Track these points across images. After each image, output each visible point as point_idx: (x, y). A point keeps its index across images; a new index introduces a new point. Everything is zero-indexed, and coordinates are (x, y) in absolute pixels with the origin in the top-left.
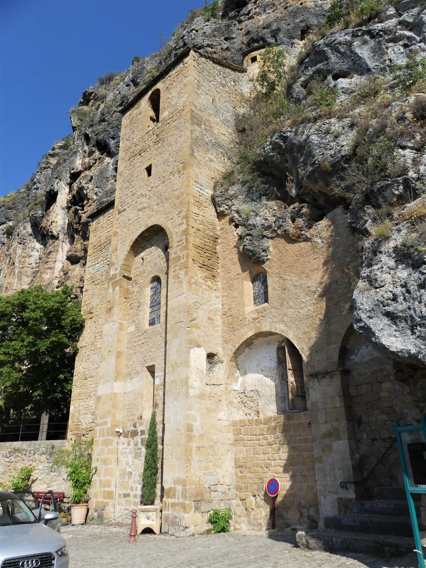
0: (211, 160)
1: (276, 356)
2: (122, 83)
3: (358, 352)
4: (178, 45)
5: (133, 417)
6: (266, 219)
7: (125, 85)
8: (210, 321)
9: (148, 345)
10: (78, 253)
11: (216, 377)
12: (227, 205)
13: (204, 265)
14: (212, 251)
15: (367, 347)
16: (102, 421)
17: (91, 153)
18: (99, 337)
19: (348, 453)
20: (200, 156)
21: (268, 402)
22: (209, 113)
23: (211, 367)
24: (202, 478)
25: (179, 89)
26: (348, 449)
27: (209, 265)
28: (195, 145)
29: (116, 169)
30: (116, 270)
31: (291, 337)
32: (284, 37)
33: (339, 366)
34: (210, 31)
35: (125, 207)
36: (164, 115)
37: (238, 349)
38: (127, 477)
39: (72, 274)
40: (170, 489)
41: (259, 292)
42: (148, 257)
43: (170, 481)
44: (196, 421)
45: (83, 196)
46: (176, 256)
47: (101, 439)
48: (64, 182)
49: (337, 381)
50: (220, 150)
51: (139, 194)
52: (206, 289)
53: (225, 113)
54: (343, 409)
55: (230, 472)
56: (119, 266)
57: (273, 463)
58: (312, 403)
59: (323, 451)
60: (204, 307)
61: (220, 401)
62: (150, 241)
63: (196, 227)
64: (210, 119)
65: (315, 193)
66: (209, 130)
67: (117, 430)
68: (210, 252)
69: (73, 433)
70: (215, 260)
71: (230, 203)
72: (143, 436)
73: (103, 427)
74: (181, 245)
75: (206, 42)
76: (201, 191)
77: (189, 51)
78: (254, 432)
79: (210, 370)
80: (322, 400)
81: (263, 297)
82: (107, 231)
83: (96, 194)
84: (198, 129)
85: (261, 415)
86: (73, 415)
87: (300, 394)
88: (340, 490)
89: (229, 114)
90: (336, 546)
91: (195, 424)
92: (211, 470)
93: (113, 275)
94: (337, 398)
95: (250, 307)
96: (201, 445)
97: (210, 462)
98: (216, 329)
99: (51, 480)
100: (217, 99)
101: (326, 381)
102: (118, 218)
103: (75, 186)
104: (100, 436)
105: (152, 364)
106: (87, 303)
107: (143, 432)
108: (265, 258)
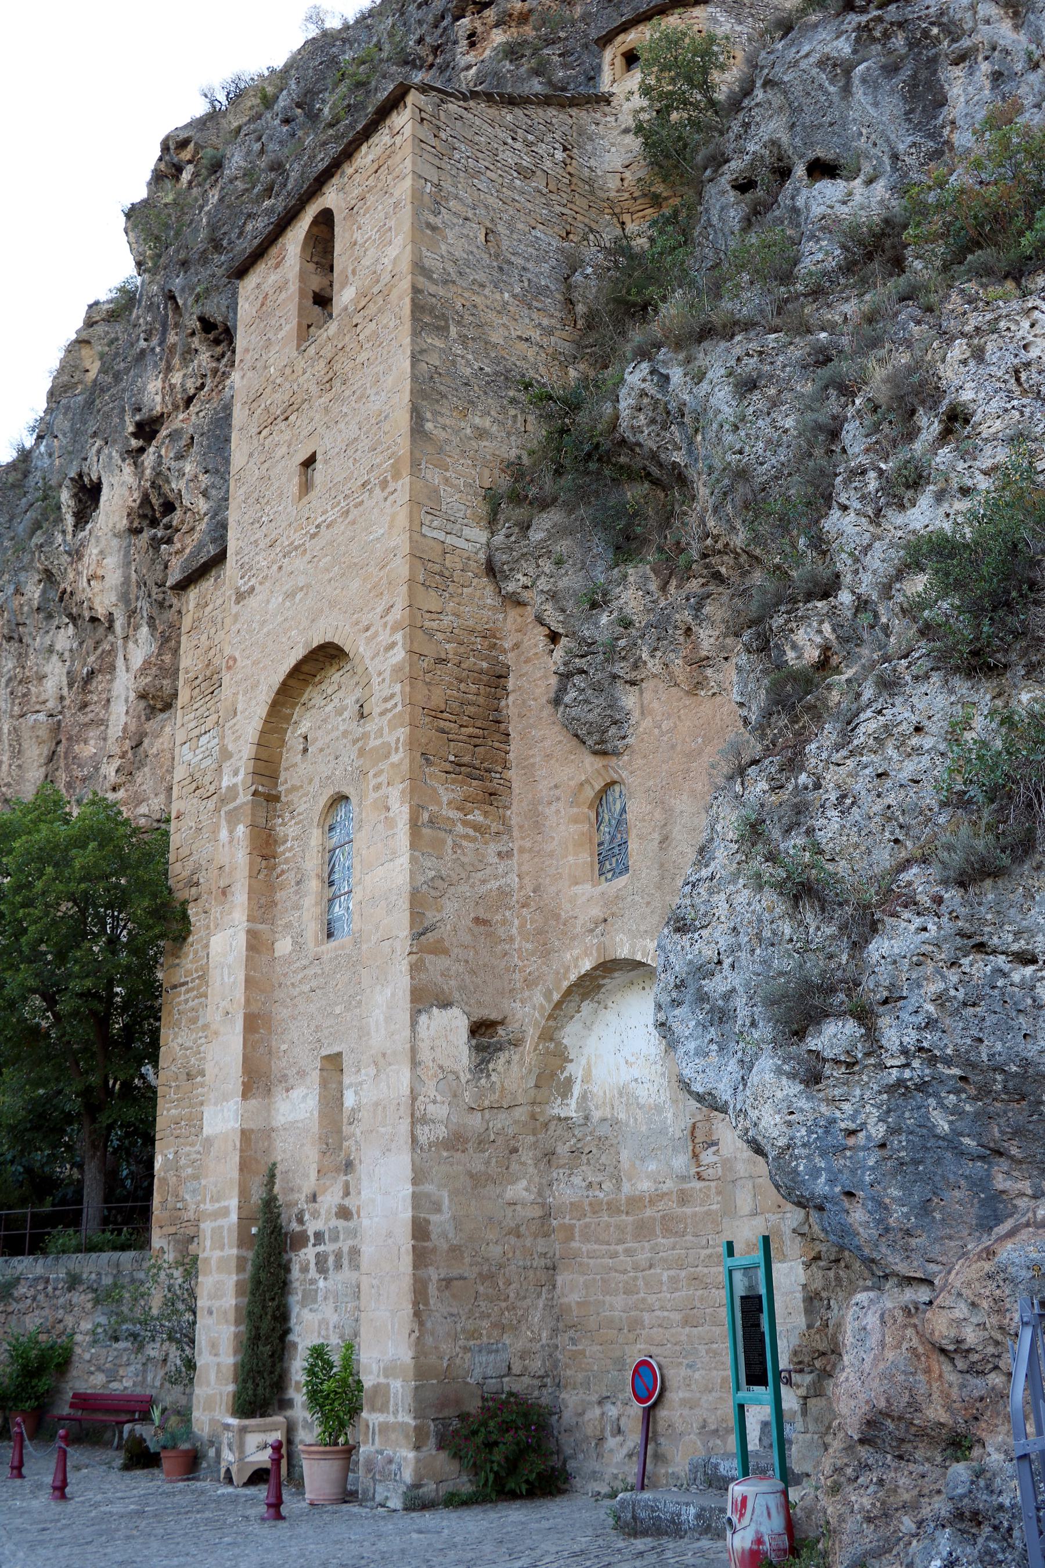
7: (277, 122)
9: (324, 994)
11: (498, 1085)
16: (217, 1205)
23: (482, 1062)
24: (458, 1361)
25: (382, 215)
27: (476, 763)
30: (236, 773)
36: (344, 297)
37: (558, 1005)
39: (152, 744)
40: (377, 1387)
43: (375, 1367)
44: (439, 1210)
45: (171, 496)
46: (378, 742)
47: (217, 1253)
52: (466, 837)
53: (530, 265)
55: (544, 1341)
56: (242, 763)
57: (646, 1316)
60: (464, 888)
61: (515, 1150)
62: (323, 686)
68: (479, 724)
70: (496, 745)
73: (220, 1222)
74: (390, 710)
83: (205, 494)
84: (439, 343)
86: (164, 1180)
91: (434, 1218)
92: (485, 1339)
93: (228, 787)
96: (455, 1273)
97: (484, 1316)
99: (117, 1362)
100: (501, 229)
103: (149, 459)
105: (336, 1049)
108: (620, 744)
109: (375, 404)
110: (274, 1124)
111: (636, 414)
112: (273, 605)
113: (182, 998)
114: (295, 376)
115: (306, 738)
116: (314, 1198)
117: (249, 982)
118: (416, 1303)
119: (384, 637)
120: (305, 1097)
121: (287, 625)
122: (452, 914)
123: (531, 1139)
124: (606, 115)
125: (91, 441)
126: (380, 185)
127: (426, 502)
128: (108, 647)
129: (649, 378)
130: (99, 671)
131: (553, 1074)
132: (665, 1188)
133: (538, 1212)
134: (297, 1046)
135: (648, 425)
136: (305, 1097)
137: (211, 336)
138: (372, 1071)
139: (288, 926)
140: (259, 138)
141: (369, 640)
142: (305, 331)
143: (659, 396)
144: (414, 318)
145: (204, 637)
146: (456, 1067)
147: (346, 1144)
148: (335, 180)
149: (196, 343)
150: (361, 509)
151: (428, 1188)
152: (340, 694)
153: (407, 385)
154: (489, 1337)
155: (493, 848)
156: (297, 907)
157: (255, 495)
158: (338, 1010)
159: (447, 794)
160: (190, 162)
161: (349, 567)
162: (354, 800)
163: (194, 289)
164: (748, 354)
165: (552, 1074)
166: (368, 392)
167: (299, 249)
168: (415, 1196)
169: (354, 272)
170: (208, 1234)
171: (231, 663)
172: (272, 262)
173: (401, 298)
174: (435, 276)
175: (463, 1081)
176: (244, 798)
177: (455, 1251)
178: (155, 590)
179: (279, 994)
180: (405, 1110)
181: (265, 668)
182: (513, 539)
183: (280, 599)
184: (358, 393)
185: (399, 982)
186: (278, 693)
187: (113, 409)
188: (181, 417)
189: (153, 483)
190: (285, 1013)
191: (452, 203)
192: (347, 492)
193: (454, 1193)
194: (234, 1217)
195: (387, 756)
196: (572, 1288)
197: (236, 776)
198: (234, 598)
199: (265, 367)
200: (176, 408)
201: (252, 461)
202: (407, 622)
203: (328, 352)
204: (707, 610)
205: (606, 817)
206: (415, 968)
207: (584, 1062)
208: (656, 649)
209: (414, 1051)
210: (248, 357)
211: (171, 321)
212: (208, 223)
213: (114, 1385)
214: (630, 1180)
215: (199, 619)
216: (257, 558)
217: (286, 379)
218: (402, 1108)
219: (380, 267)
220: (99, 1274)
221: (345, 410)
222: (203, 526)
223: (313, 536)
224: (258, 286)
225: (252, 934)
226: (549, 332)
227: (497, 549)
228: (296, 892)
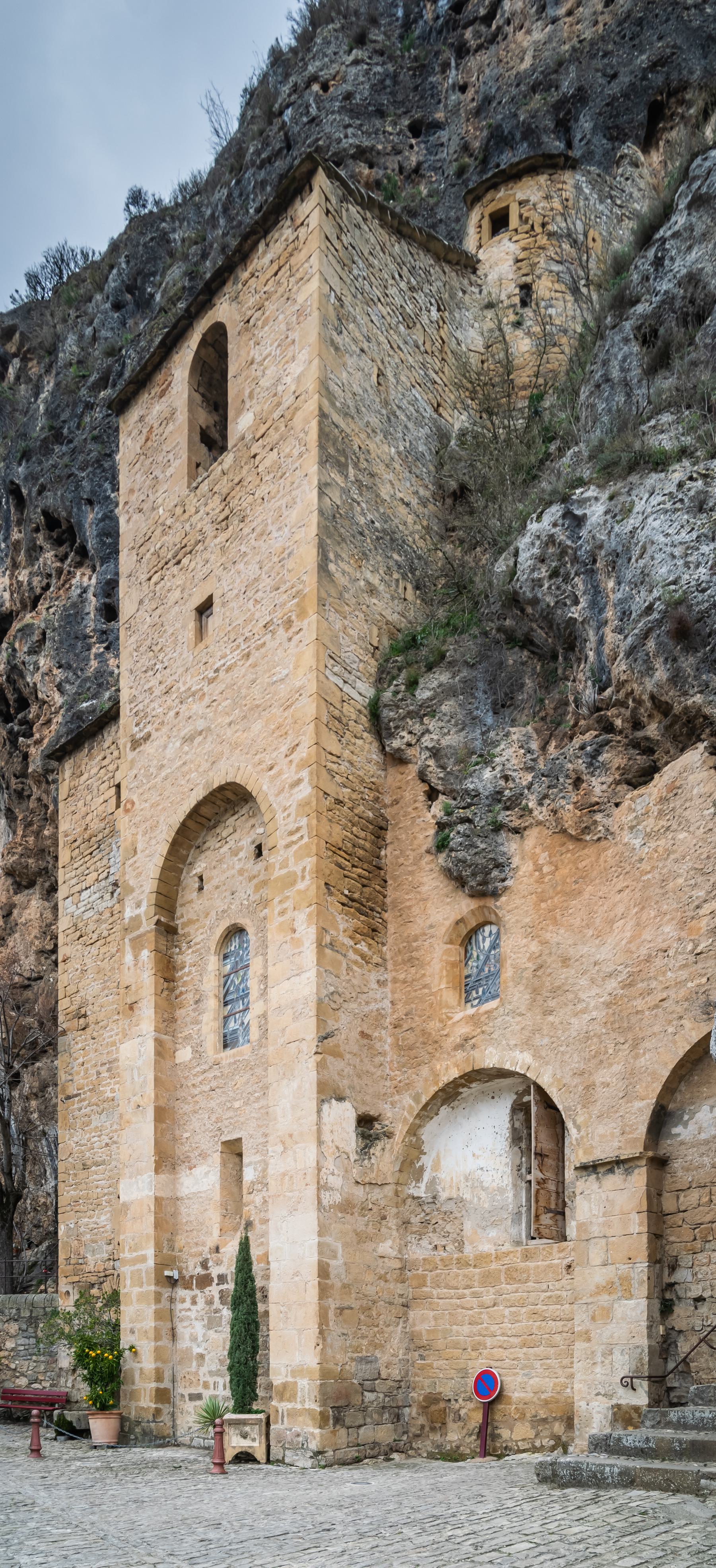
0: (372, 590)
1: (508, 1125)
2: (98, 297)
3: (691, 1118)
4: (266, 144)
5: (200, 1249)
6: (506, 778)
7: (108, 305)
8: (365, 1041)
12: (410, 733)
13: (353, 900)
14: (370, 863)
17: (34, 552)
18: (106, 1074)
19: (644, 1324)
20: (344, 572)
22: (368, 422)
25: (283, 327)
26: (645, 1316)
28: (330, 536)
29: (110, 612)
30: (138, 905)
31: (545, 1081)
32: (594, 129)
33: (646, 1148)
34: (365, 90)
35: (149, 728)
36: (241, 424)
38: (194, 1364)
40: (285, 1386)
41: (478, 974)
43: (283, 1370)
44: (335, 1257)
45: (26, 692)
46: (284, 872)
47: (136, 1290)
49: (639, 1178)
50: (396, 556)
51: (183, 689)
52: (356, 962)
53: (410, 425)
54: (644, 1238)
57: (489, 1341)
58: (581, 1227)
59: (593, 1318)
60: (353, 1006)
61: (384, 1218)
62: (218, 830)
63: (333, 794)
64: (372, 447)
65: (639, 702)
66: (368, 485)
67: (167, 1273)
68: (365, 866)
69: (70, 1279)
72: (224, 1287)
73: (138, 1266)
74: (294, 843)
75: (351, 140)
76: (347, 688)
77: (312, 173)
78: (453, 1283)
79: (364, 1151)
80: (601, 1220)
82: (101, 799)
83: (60, 688)
84: (339, 479)
85: (468, 1249)
87: (553, 1206)
88: (621, 1391)
89: (424, 432)
90: (610, 1480)
91: (333, 1263)
93: (131, 918)
94: (635, 1218)
96: (346, 1304)
98: (378, 1059)
100: (389, 373)
101: (615, 1180)
102: (133, 762)
104: (133, 1285)
106: (72, 989)
107: (222, 1279)
108: (500, 885)
109: (278, 540)
110: (179, 1195)
111: (539, 565)
112: (170, 752)
114: (186, 516)
115: (201, 878)
116: (217, 1250)
117: (157, 1081)
118: (320, 1325)
119: (290, 775)
120: (207, 1173)
121: (186, 768)
122: (345, 1025)
123: (394, 1210)
124: (471, 284)
126: (281, 290)
129: (560, 522)
131: (412, 1163)
132: (504, 1249)
133: (398, 1264)
134: (200, 1133)
135: (551, 577)
136: (207, 1173)
137: (55, 534)
138: (280, 1148)
139: (188, 1038)
140: (91, 323)
141: (273, 778)
142: (196, 467)
143: (569, 543)
144: (322, 447)
145: (81, 804)
146: (347, 1149)
147: (246, 1209)
148: (229, 288)
149: (40, 539)
150: (263, 650)
151: (328, 1239)
152: (236, 836)
153: (315, 518)
155: (373, 977)
156: (197, 1022)
157: (148, 643)
158: (237, 1105)
159: (343, 924)
160: (15, 355)
161: (252, 709)
162: (251, 930)
163: (37, 479)
164: (691, 478)
165: (410, 1164)
166: (270, 528)
167: (186, 373)
168: (320, 1245)
169: (251, 396)
170: (128, 1276)
172: (155, 390)
173: (307, 421)
176: (148, 926)
178: (13, 781)
179: (181, 1094)
180: (311, 1179)
181: (164, 809)
182: (400, 696)
183: (178, 744)
184: (258, 530)
185: (306, 1076)
186: (177, 833)
188: (28, 616)
189: (8, 677)
190: (187, 1108)
192: (247, 635)
193: (346, 1245)
194: (151, 1263)
195: (293, 883)
196: (422, 1320)
197: (140, 907)
198: (129, 745)
199: (154, 509)
200: (24, 607)
201: (143, 608)
202: (314, 760)
203: (223, 486)
204: (604, 757)
205: (475, 954)
206: (321, 1066)
207: (434, 1155)
208: (546, 796)
209: (319, 1132)
210: (133, 498)
211: (13, 517)
212: (47, 410)
213: (36, 1386)
214: (471, 1243)
215: (75, 788)
216: (152, 705)
217: (177, 520)
218: (308, 1178)
219: (280, 388)
220: (18, 1309)
222: (59, 718)
223: (211, 681)
224: (142, 419)
225: (158, 1042)
226: (424, 503)
227: (386, 706)
228: (194, 1010)
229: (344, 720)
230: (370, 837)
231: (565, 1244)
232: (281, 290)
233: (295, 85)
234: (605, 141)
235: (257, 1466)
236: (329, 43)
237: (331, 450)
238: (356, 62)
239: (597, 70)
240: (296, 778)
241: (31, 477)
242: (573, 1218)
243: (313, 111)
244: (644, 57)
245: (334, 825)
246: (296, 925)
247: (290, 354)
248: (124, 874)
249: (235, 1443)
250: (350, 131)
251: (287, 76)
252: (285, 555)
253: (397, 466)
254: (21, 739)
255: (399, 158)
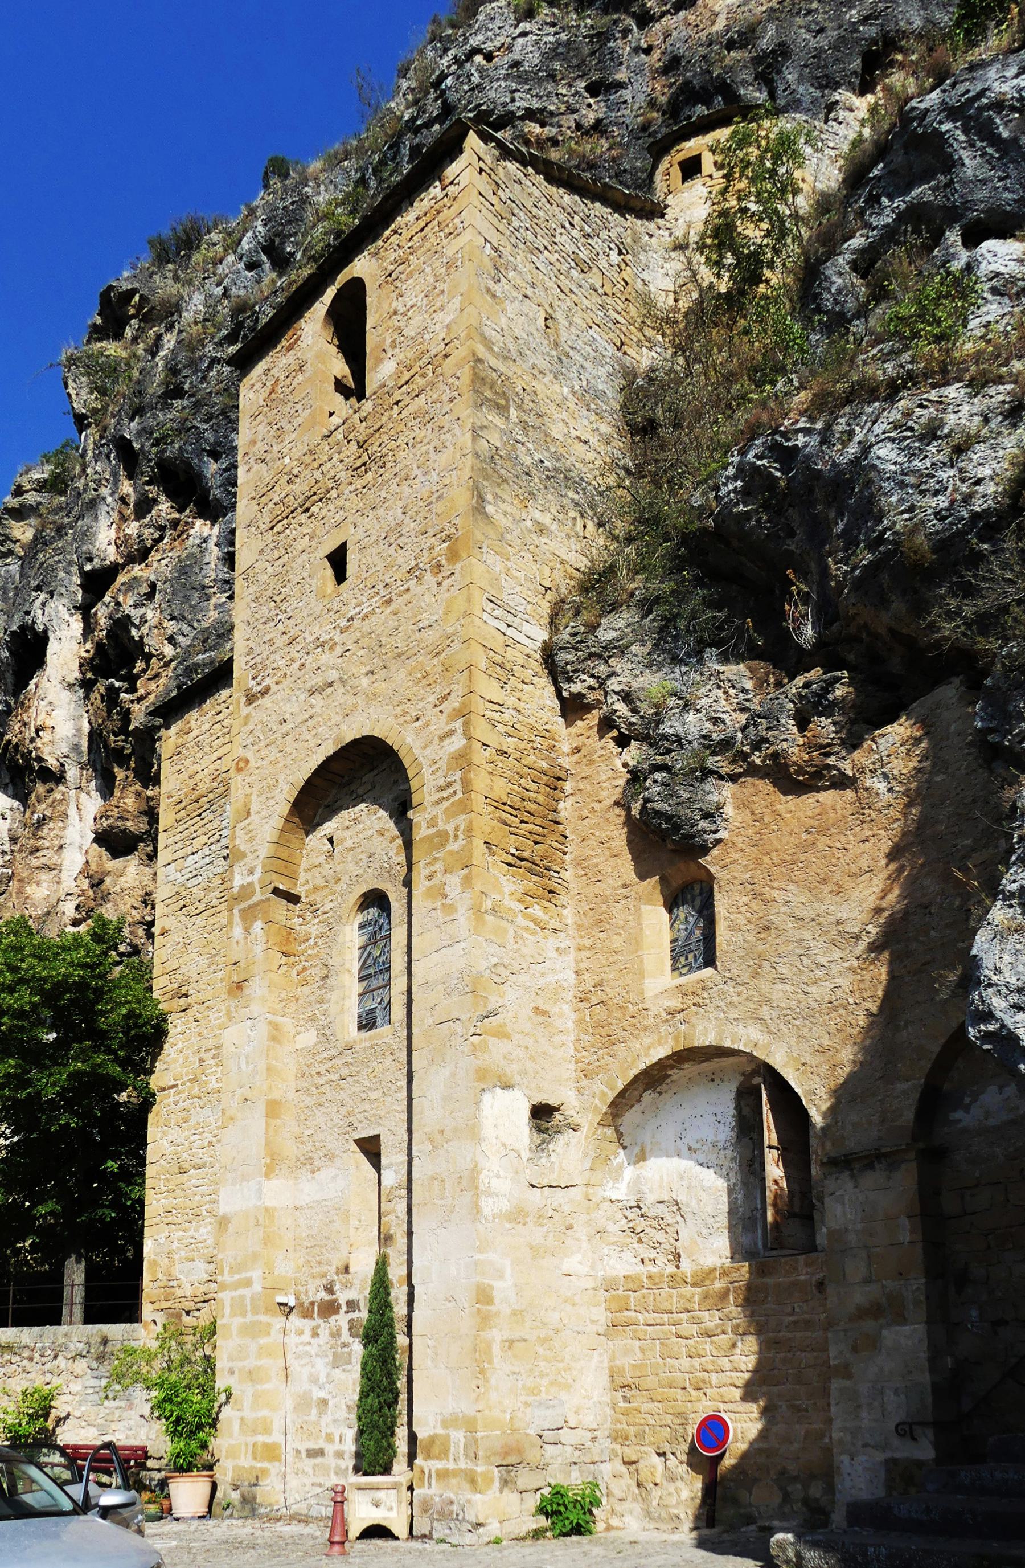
1: (733, 1112)
4: (422, 110)
5: (325, 1268)
8: (541, 1019)
10: (129, 824)
13: (522, 860)
14: (545, 818)
15: (1001, 1089)
16: (236, 1277)
18: (212, 1062)
20: (505, 514)
21: (705, 1232)
23: (543, 1142)
24: (520, 1414)
25: (431, 279)
27: (537, 860)
29: (230, 560)
30: (251, 872)
31: (779, 1060)
32: (800, 80)
34: (535, 58)
36: (380, 373)
38: (314, 1411)
40: (433, 1440)
41: (688, 937)
42: (348, 833)
44: (501, 1277)
47: (238, 1321)
48: (65, 601)
50: (571, 494)
51: (310, 639)
52: (527, 929)
53: (588, 365)
54: (919, 1249)
55: (596, 1399)
59: (855, 1349)
60: (522, 978)
61: (570, 1227)
62: (353, 787)
64: (539, 387)
66: (535, 424)
68: (538, 821)
69: (157, 1306)
70: (555, 844)
71: (602, 669)
72: (355, 1315)
74: (447, 799)
75: (523, 101)
76: (509, 632)
81: (701, 949)
83: (171, 640)
84: (498, 421)
87: (797, 1210)
88: (896, 1441)
89: (603, 372)
91: (496, 1284)
92: (544, 1395)
93: (242, 886)
94: (905, 1221)
95: (659, 980)
96: (516, 1335)
100: (559, 315)
104: (233, 1315)
106: (169, 966)
107: (352, 1306)
108: (711, 837)
113: (171, 1099)
121: (310, 723)
125: (34, 594)
127: (489, 588)
128: (59, 796)
130: (51, 819)
154: (547, 1394)
158: (373, 1095)
163: (152, 434)
170: (227, 1303)
171: (242, 764)
174: (495, 349)
175: (525, 1159)
177: (517, 1315)
187: (59, 561)
188: (137, 567)
191: (511, 274)
192: (388, 581)
221: (383, 494)
229: (508, 666)
230: (544, 789)
231: (814, 1255)
232: (428, 245)
233: (455, 57)
234: (812, 90)
235: (391, 1543)
236: (493, 19)
237: (488, 394)
238: (524, 34)
239: (800, 27)
240: (447, 728)
241: (145, 432)
242: (823, 1222)
243: (476, 79)
244: (854, 12)
245: (496, 779)
246: (447, 889)
247: (439, 304)
248: (234, 838)
249: (362, 1513)
250: (517, 95)
251: (446, 50)
252: (433, 499)
253: (572, 406)
254: (123, 695)
255: (576, 116)
